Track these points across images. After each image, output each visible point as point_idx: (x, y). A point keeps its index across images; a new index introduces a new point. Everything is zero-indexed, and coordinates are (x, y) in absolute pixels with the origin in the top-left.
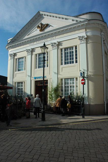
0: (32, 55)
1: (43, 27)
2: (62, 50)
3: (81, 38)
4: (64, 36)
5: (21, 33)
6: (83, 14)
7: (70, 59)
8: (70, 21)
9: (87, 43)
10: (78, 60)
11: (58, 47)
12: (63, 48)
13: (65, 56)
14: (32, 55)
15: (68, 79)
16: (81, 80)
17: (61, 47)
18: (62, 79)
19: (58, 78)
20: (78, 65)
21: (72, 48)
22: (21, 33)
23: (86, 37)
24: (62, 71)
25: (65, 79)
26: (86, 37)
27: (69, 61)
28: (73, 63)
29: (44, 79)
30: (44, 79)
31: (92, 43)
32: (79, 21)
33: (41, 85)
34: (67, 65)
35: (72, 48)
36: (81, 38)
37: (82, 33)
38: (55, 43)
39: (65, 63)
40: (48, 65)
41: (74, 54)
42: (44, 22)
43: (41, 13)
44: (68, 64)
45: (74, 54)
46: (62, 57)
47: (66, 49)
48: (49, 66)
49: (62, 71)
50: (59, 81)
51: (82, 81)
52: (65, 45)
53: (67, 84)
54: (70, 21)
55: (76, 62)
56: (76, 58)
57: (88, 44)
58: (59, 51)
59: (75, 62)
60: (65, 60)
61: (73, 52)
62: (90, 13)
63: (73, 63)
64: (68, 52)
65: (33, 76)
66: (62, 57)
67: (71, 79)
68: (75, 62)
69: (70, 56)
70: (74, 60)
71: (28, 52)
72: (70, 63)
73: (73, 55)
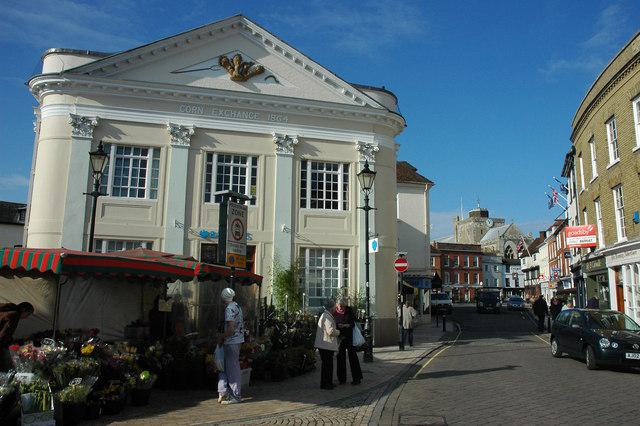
1: (246, 72)
2: (210, 156)
5: (135, 54)
6: (373, 89)
7: (328, 196)
8: (339, 93)
12: (248, 155)
15: (320, 251)
18: (303, 250)
19: (293, 244)
20: (160, 204)
22: (135, 54)
24: (103, 214)
25: (312, 250)
27: (324, 199)
28: (142, 194)
32: (364, 104)
34: (317, 211)
36: (364, 149)
38: (184, 129)
39: (313, 205)
40: (345, 204)
41: (340, 183)
45: (340, 183)
49: (103, 214)
50: (297, 253)
52: (227, 145)
55: (153, 194)
58: (299, 164)
59: (340, 206)
60: (313, 194)
61: (144, 163)
63: (142, 194)
65: (194, 226)
69: (328, 187)
70: (147, 187)
71: (177, 136)
72: (328, 207)
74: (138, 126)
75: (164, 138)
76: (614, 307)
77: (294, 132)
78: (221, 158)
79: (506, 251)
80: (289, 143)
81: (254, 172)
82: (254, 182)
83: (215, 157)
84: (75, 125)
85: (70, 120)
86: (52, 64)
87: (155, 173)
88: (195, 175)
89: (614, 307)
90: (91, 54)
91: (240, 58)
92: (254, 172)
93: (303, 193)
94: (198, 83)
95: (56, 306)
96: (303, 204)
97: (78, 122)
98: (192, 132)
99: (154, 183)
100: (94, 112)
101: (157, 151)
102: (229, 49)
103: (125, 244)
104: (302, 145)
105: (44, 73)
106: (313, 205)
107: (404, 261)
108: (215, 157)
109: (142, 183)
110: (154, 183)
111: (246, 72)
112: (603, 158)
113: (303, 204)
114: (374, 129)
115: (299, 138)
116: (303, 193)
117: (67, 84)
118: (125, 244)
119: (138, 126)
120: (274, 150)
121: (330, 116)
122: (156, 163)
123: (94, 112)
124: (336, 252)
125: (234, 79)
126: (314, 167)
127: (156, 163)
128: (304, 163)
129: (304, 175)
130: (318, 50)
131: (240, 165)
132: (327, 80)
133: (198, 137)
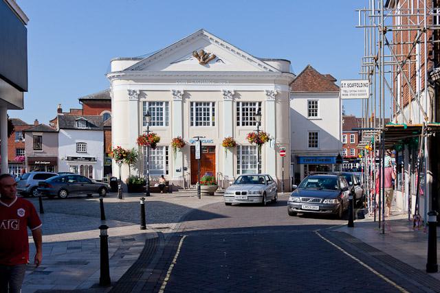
0: (183, 102)
1: (205, 59)
3: (268, 94)
5: (158, 55)
6: (274, 60)
7: (158, 119)
8: (254, 67)
9: (276, 102)
10: (170, 121)
11: (139, 98)
13: (197, 114)
14: (183, 102)
17: (142, 99)
23: (276, 93)
26: (276, 93)
27: (156, 121)
35: (162, 103)
36: (268, 94)
37: (271, 87)
39: (197, 124)
42: (210, 49)
43: (205, 33)
44: (247, 125)
45: (211, 110)
48: (170, 123)
54: (254, 67)
55: (167, 124)
57: (277, 104)
58: (235, 104)
59: (164, 124)
61: (162, 109)
62: (278, 60)
64: (154, 108)
68: (211, 124)
70: (164, 121)
72: (251, 124)
74: (157, 92)
75: (167, 97)
76: (185, 156)
77: (232, 88)
78: (150, 103)
80: (229, 94)
81: (213, 110)
82: (213, 115)
83: (241, 104)
84: (130, 94)
85: (128, 92)
86: (117, 66)
87: (167, 114)
88: (281, 118)
89: (185, 156)
90: (135, 59)
92: (213, 110)
93: (238, 119)
94: (165, 70)
96: (238, 124)
97: (131, 93)
98: (233, 93)
99: (167, 119)
100: (138, 87)
101: (167, 103)
102: (196, 47)
104: (236, 94)
105: (113, 70)
107: (284, 151)
109: (162, 119)
110: (167, 119)
111: (205, 59)
113: (238, 124)
114: (275, 82)
115: (235, 91)
116: (238, 119)
117: (126, 74)
119: (157, 92)
120: (266, 98)
121: (165, 78)
122: (167, 109)
123: (138, 87)
125: (202, 63)
127: (167, 109)
128: (238, 104)
129: (192, 109)
130: (239, 45)
131: (206, 107)
132: (248, 59)
133: (186, 95)
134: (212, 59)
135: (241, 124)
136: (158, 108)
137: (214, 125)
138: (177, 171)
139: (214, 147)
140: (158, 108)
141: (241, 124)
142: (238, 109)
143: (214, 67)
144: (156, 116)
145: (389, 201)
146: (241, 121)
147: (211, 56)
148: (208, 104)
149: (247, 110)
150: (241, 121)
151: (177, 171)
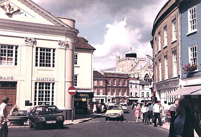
2: (37, 49)
4: (63, 18)
7: (47, 62)
13: (41, 58)
16: (67, 89)
21: (49, 50)
27: (45, 63)
28: (50, 66)
29: (101, 87)
30: (101, 87)
31: (71, 51)
33: (96, 114)
34: (42, 68)
37: (63, 39)
39: (41, 65)
44: (44, 66)
46: (37, 57)
47: (42, 49)
51: (70, 89)
52: (40, 44)
53: (47, 91)
55: (53, 66)
56: (54, 62)
58: (34, 49)
59: (51, 65)
60: (41, 61)
63: (50, 66)
66: (37, 57)
67: (46, 84)
68: (51, 65)
69: (47, 58)
70: (51, 63)
72: (46, 66)
73: (50, 58)
79: (145, 77)
91: (9, 5)
93: (37, 61)
95: (81, 99)
101: (54, 50)
103: (45, 83)
106: (41, 65)
108: (39, 49)
112: (170, 36)
113: (36, 65)
116: (37, 61)
118: (45, 83)
124: (49, 84)
126: (41, 50)
134: (16, 11)
135: (39, 65)
136: (47, 54)
137: (16, 64)
138: (136, 94)
139: (13, 85)
140: (47, 54)
141: (39, 65)
142: (37, 53)
143: (16, 18)
144: (45, 60)
145: (197, 105)
146: (39, 63)
147: (15, 9)
148: (12, 47)
149: (44, 54)
150: (39, 63)
151: (136, 94)
